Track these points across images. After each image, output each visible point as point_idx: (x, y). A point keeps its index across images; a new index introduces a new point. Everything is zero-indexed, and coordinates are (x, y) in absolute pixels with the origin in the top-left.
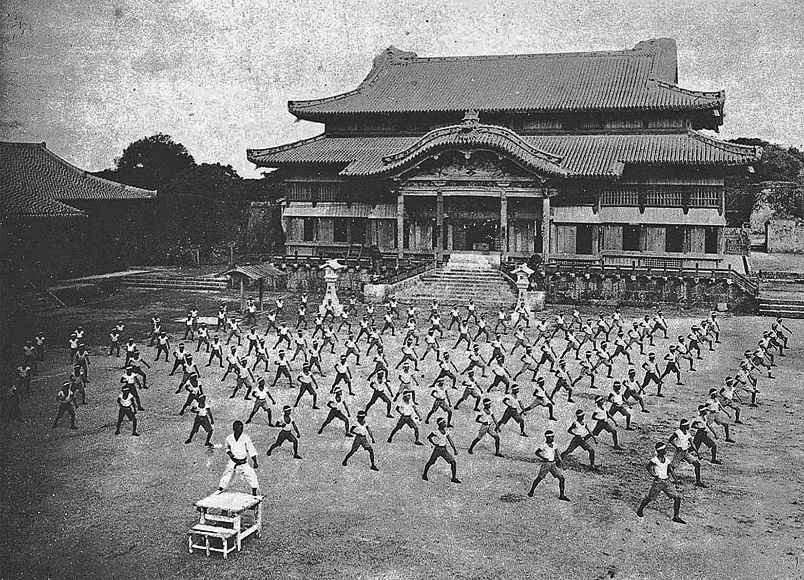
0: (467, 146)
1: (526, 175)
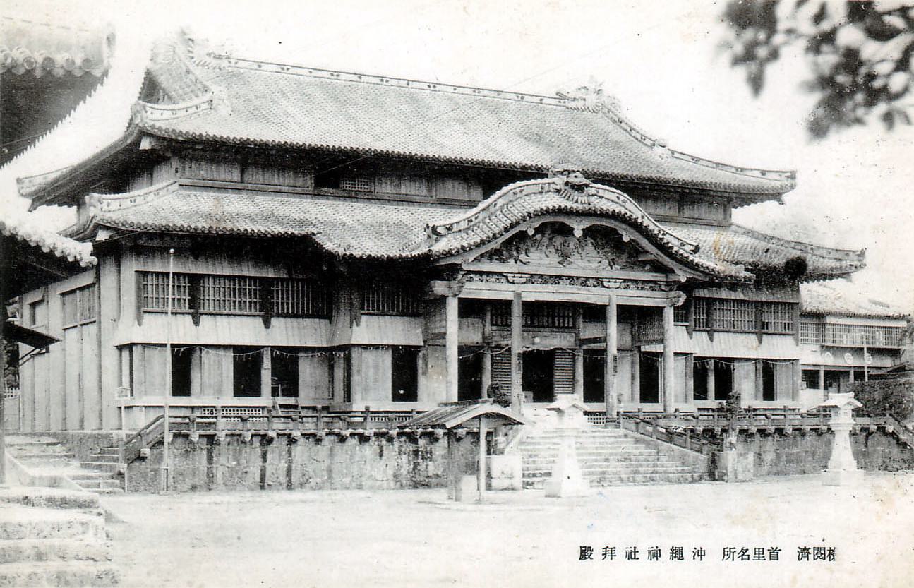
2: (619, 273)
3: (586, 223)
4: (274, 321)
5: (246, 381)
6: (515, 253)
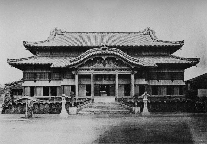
0: (105, 55)
1: (125, 65)
2: (118, 67)
3: (106, 57)
4: (51, 81)
5: (46, 93)
6: (92, 65)
